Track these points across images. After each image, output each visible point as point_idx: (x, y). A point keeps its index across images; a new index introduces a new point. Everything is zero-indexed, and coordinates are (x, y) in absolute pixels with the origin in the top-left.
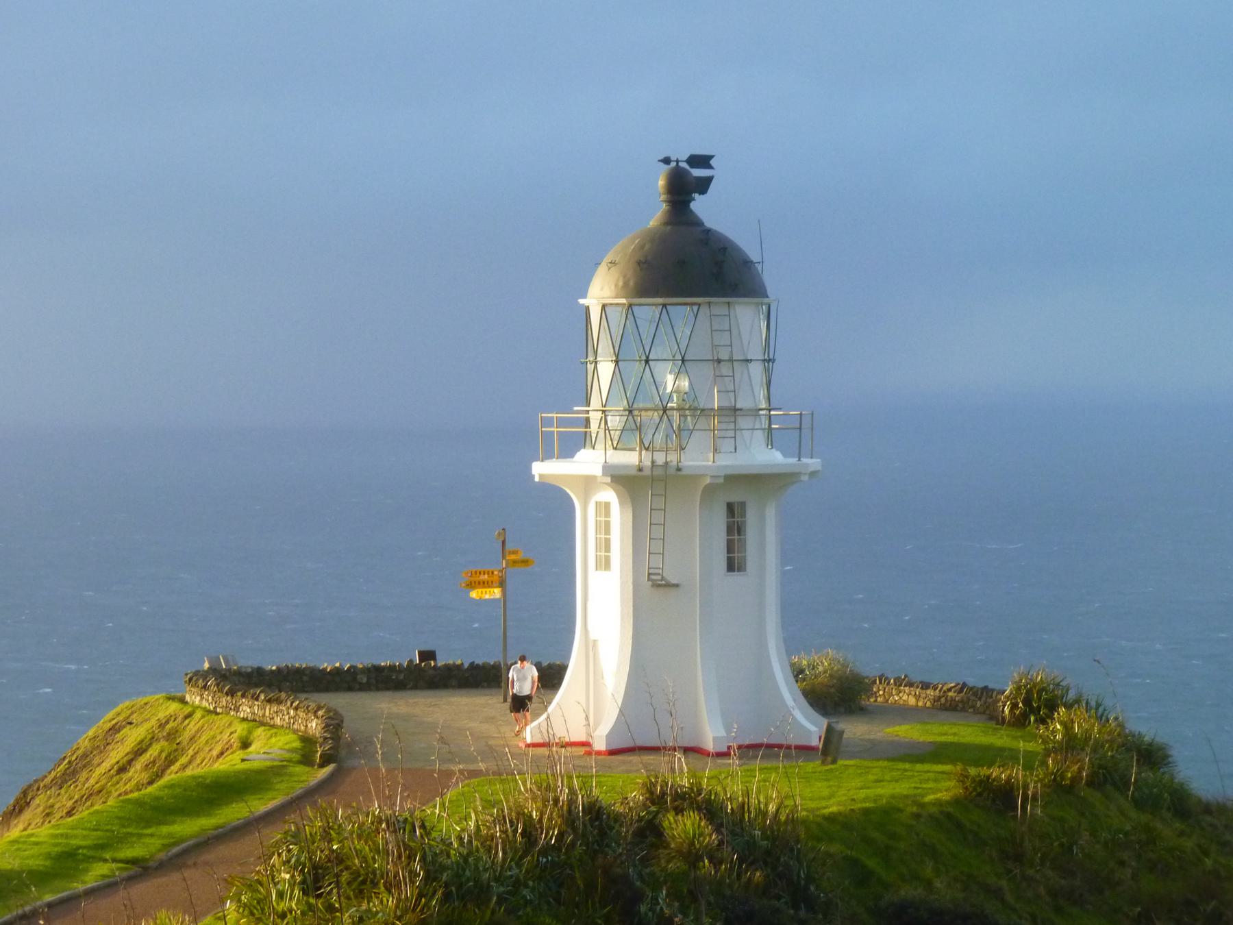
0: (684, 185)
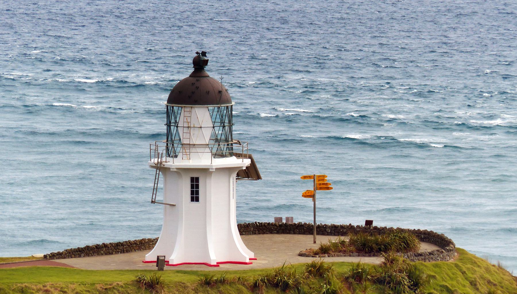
0: (200, 63)
